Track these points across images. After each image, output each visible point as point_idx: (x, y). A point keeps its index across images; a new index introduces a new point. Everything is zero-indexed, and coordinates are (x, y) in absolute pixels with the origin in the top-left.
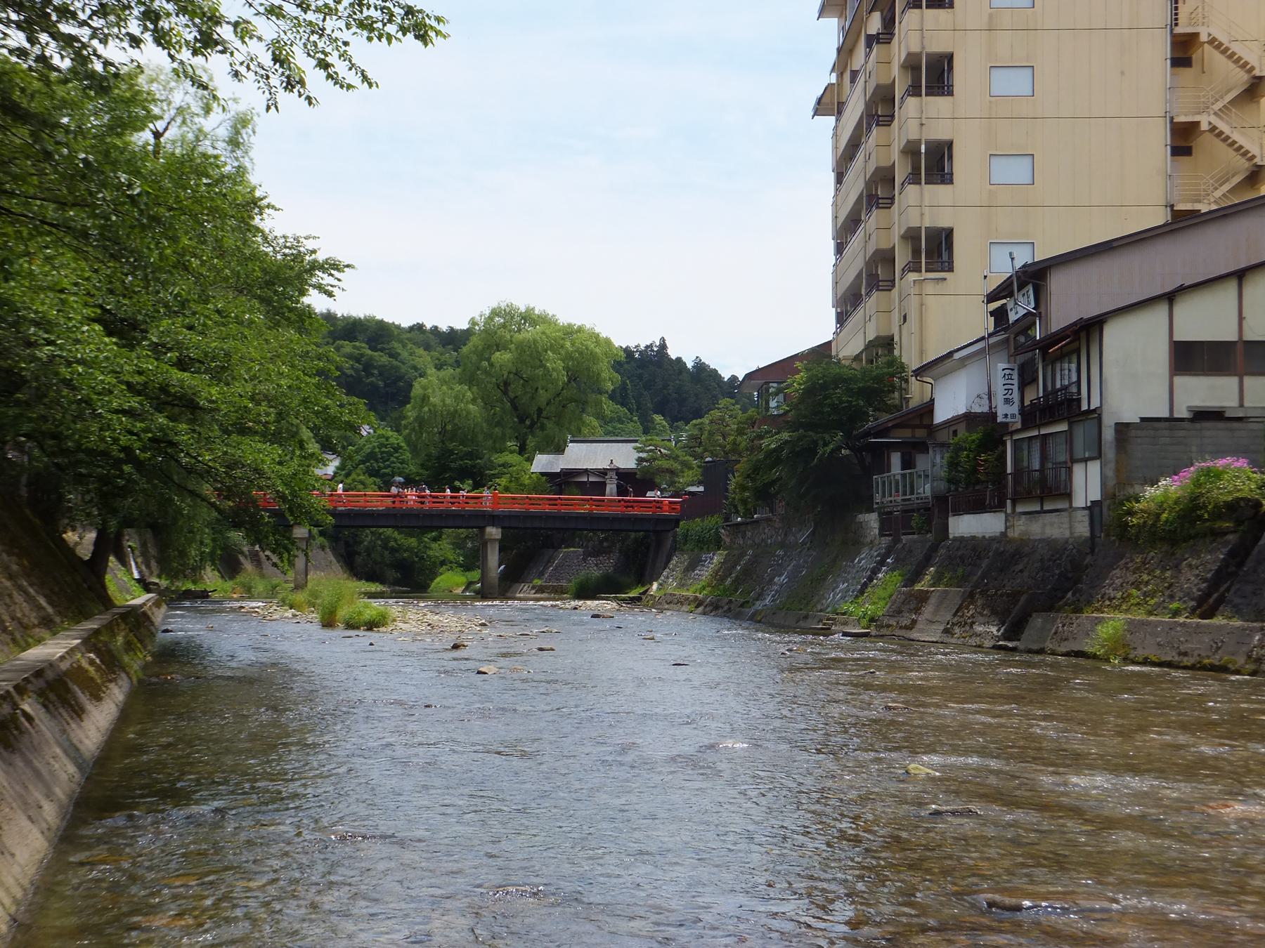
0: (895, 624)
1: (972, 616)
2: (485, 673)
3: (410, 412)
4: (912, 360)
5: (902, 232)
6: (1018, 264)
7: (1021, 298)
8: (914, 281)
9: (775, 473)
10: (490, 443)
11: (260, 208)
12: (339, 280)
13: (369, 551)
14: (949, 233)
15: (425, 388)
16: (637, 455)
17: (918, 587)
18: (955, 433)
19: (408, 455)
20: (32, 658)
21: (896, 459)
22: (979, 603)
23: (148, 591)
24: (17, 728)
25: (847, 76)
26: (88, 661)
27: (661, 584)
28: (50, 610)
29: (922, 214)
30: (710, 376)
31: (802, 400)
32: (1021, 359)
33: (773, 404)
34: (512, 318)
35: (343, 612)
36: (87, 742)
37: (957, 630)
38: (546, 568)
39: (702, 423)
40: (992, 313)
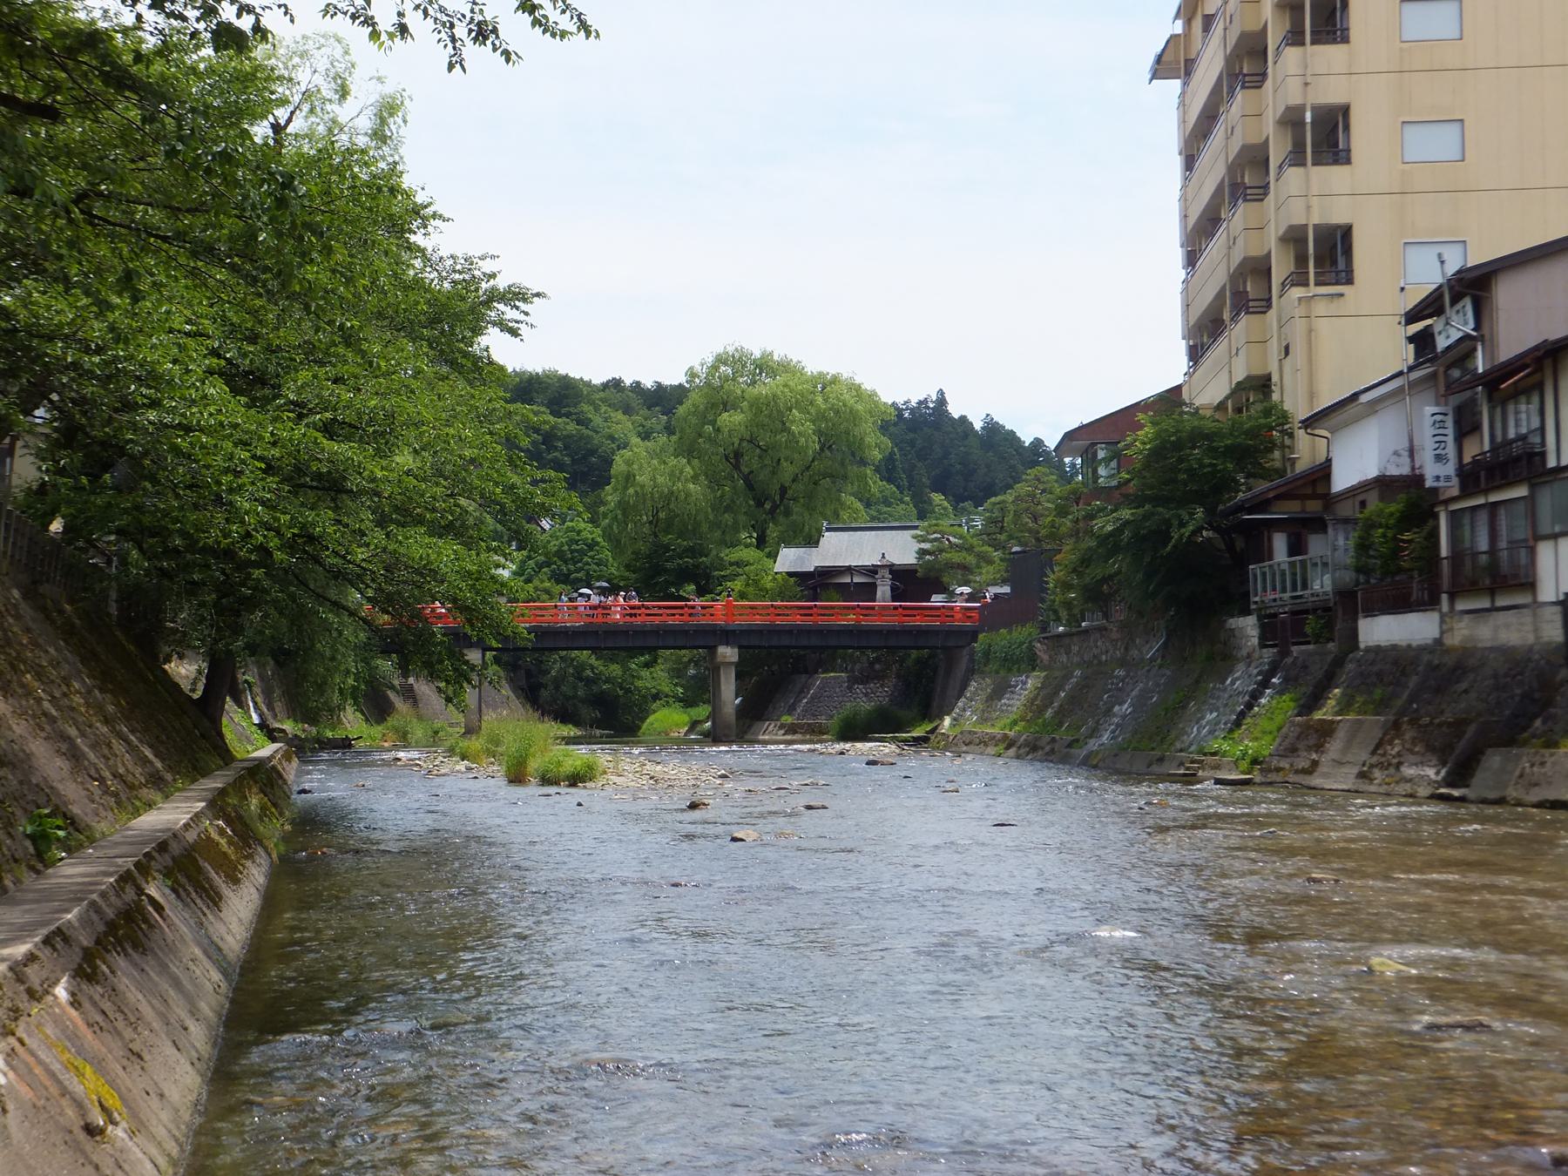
0: (1287, 766)
1: (1399, 754)
2: (742, 840)
3: (610, 495)
4: (1297, 405)
5: (1281, 232)
6: (1451, 268)
7: (1454, 317)
8: (1300, 299)
9: (1114, 565)
10: (718, 534)
11: (424, 218)
12: (527, 314)
13: (557, 685)
14: (1347, 231)
15: (629, 463)
16: (917, 546)
17: (1318, 716)
18: (1363, 504)
19: (607, 554)
20: (146, 826)
21: (1280, 543)
22: (1408, 736)
23: (274, 740)
24: (146, 921)
25: (1198, 24)
26: (214, 828)
27: (955, 719)
28: (159, 765)
29: (1308, 207)
30: (1007, 440)
31: (1147, 465)
32: (1456, 400)
33: (1102, 471)
34: (744, 366)
35: (534, 765)
36: (229, 939)
37: (1377, 773)
38: (798, 701)
39: (1004, 501)
40: (1411, 339)
